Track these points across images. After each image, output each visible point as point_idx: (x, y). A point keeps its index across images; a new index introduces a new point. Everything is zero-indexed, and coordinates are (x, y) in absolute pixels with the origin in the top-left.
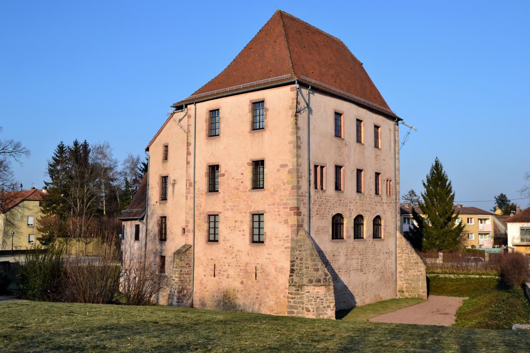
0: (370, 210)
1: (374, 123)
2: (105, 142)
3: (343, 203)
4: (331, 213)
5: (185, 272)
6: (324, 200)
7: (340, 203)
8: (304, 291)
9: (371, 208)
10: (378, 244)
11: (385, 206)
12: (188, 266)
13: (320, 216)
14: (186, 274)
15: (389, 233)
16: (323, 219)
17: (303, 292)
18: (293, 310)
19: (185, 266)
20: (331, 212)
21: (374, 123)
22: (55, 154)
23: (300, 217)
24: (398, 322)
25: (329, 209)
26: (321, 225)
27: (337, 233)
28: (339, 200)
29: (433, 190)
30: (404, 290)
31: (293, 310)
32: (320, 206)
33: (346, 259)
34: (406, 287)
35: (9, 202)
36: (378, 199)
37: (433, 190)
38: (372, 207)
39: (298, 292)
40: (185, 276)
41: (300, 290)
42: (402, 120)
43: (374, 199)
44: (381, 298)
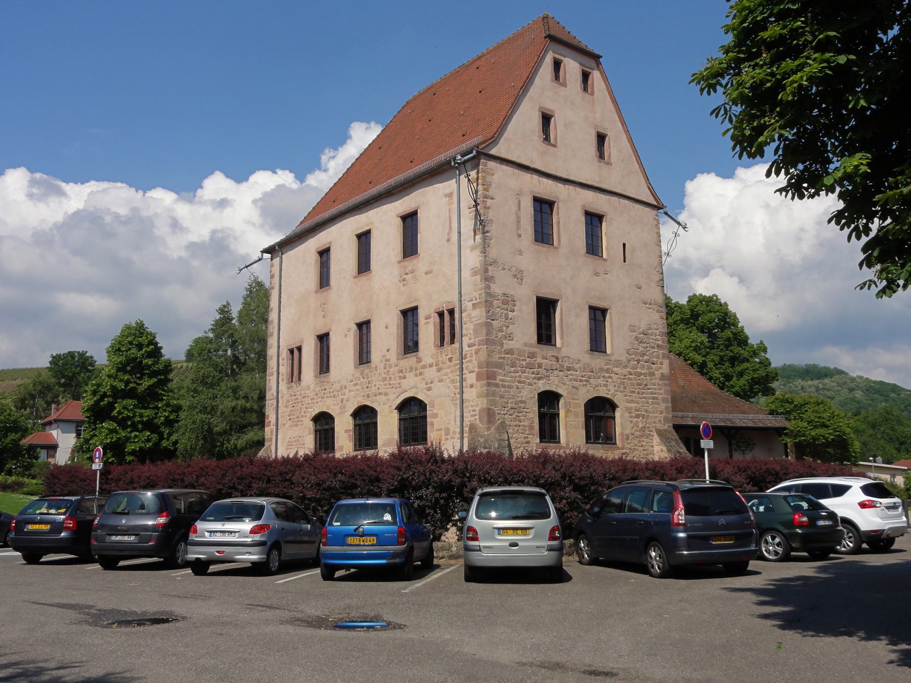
0: (383, 391)
2: (217, 310)
3: (330, 392)
4: (308, 415)
7: (324, 394)
9: (389, 386)
13: (293, 422)
15: (443, 432)
16: (296, 425)
18: (495, 370)
20: (308, 412)
21: (540, 109)
24: (878, 375)
25: (307, 408)
26: (294, 436)
27: (326, 438)
28: (322, 390)
29: (852, 57)
31: (495, 370)
32: (293, 407)
37: (852, 57)
38: (390, 384)
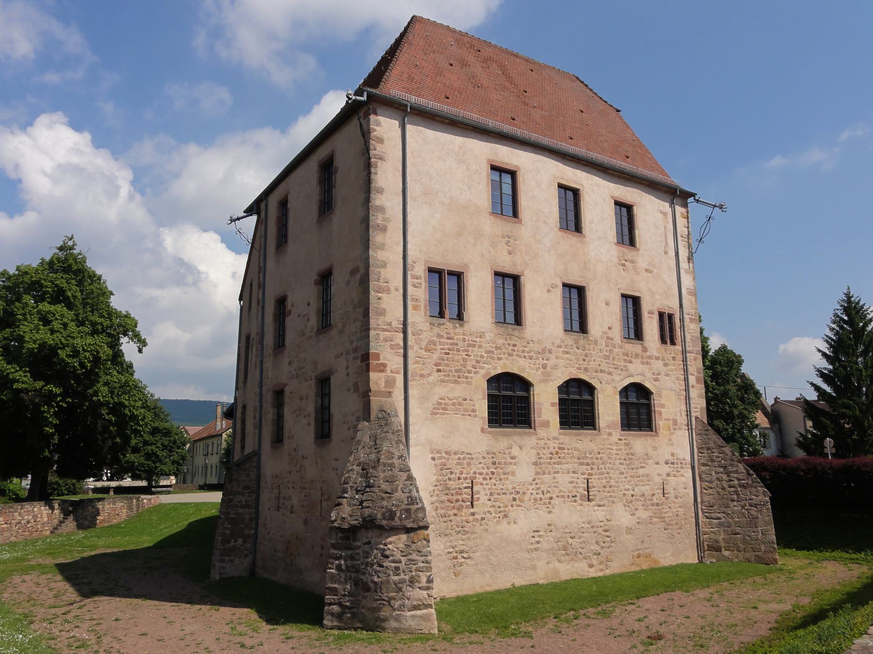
1: (488, 160)
3: (523, 351)
5: (241, 502)
6: (460, 343)
7: (514, 350)
8: (359, 540)
10: (639, 442)
11: (658, 365)
12: (247, 491)
14: (242, 507)
17: (358, 543)
19: (240, 490)
21: (488, 160)
22: (817, 388)
23: (383, 374)
30: (722, 544)
32: (447, 354)
33: (537, 473)
34: (723, 539)
35: (244, 394)
36: (634, 347)
39: (347, 542)
40: (241, 511)
41: (351, 538)
42: (693, 195)
43: (621, 347)
44: (656, 561)
